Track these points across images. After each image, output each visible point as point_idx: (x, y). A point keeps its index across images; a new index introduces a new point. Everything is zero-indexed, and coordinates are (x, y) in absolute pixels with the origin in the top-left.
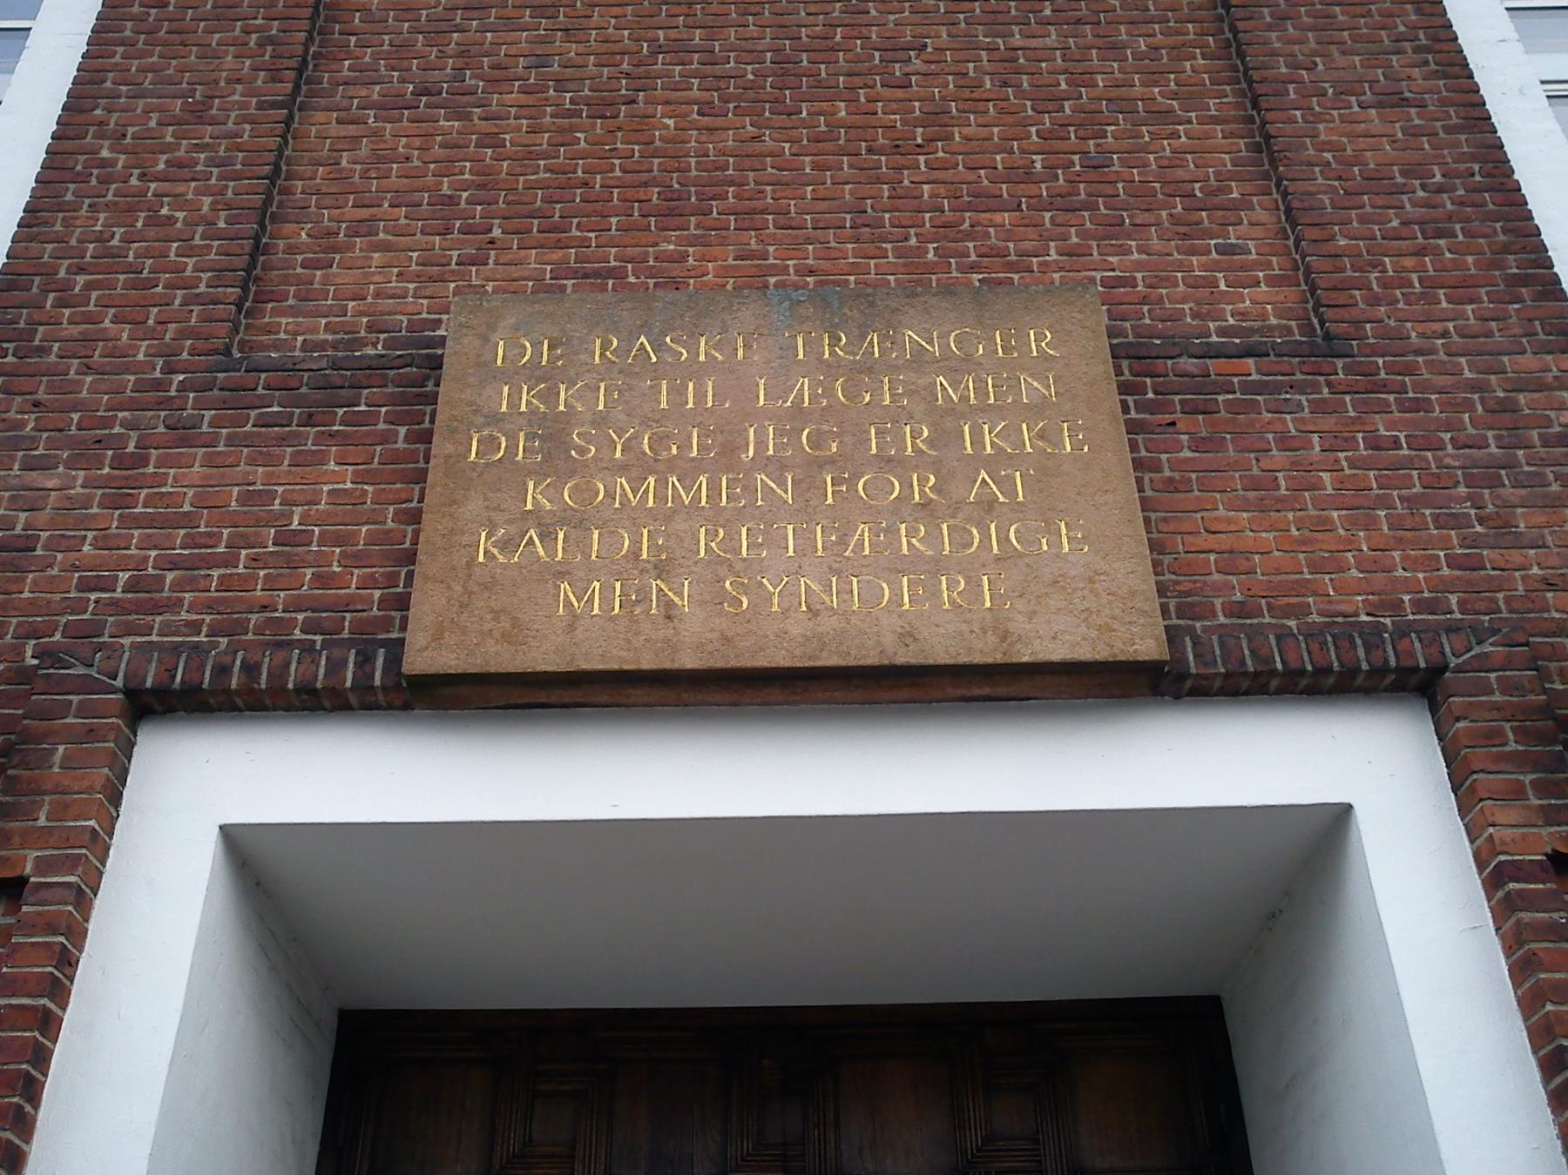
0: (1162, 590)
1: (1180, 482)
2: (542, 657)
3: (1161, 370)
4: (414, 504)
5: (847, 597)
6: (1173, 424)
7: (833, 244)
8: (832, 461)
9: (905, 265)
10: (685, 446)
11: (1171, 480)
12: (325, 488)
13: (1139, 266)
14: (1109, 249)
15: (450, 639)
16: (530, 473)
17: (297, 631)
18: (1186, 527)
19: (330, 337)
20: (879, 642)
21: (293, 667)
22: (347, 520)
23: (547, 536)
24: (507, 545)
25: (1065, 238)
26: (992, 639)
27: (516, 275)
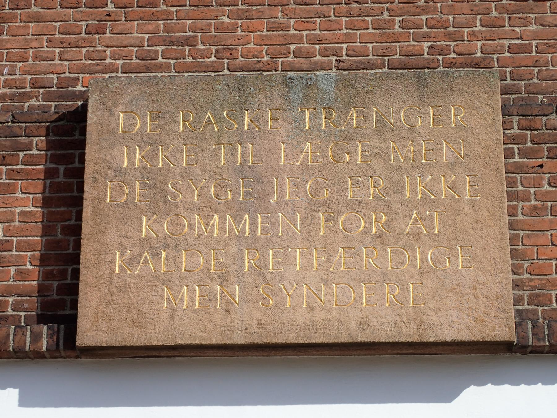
0: (517, 285)
1: (541, 209)
2: (155, 336)
3: (538, 126)
4: (73, 222)
5: (330, 298)
6: (541, 166)
7: (333, 18)
8: (325, 204)
9: (381, 35)
10: (235, 193)
11: (535, 207)
12: (18, 210)
13: (535, 36)
14: (518, 22)
15: (103, 324)
16: (142, 212)
17: (9, 309)
18: (541, 241)
19: (8, 91)
20: (348, 328)
21: (11, 337)
22: (33, 234)
23: (156, 255)
24: (132, 261)
25: (487, 12)
26: (412, 325)
27: (126, 43)
